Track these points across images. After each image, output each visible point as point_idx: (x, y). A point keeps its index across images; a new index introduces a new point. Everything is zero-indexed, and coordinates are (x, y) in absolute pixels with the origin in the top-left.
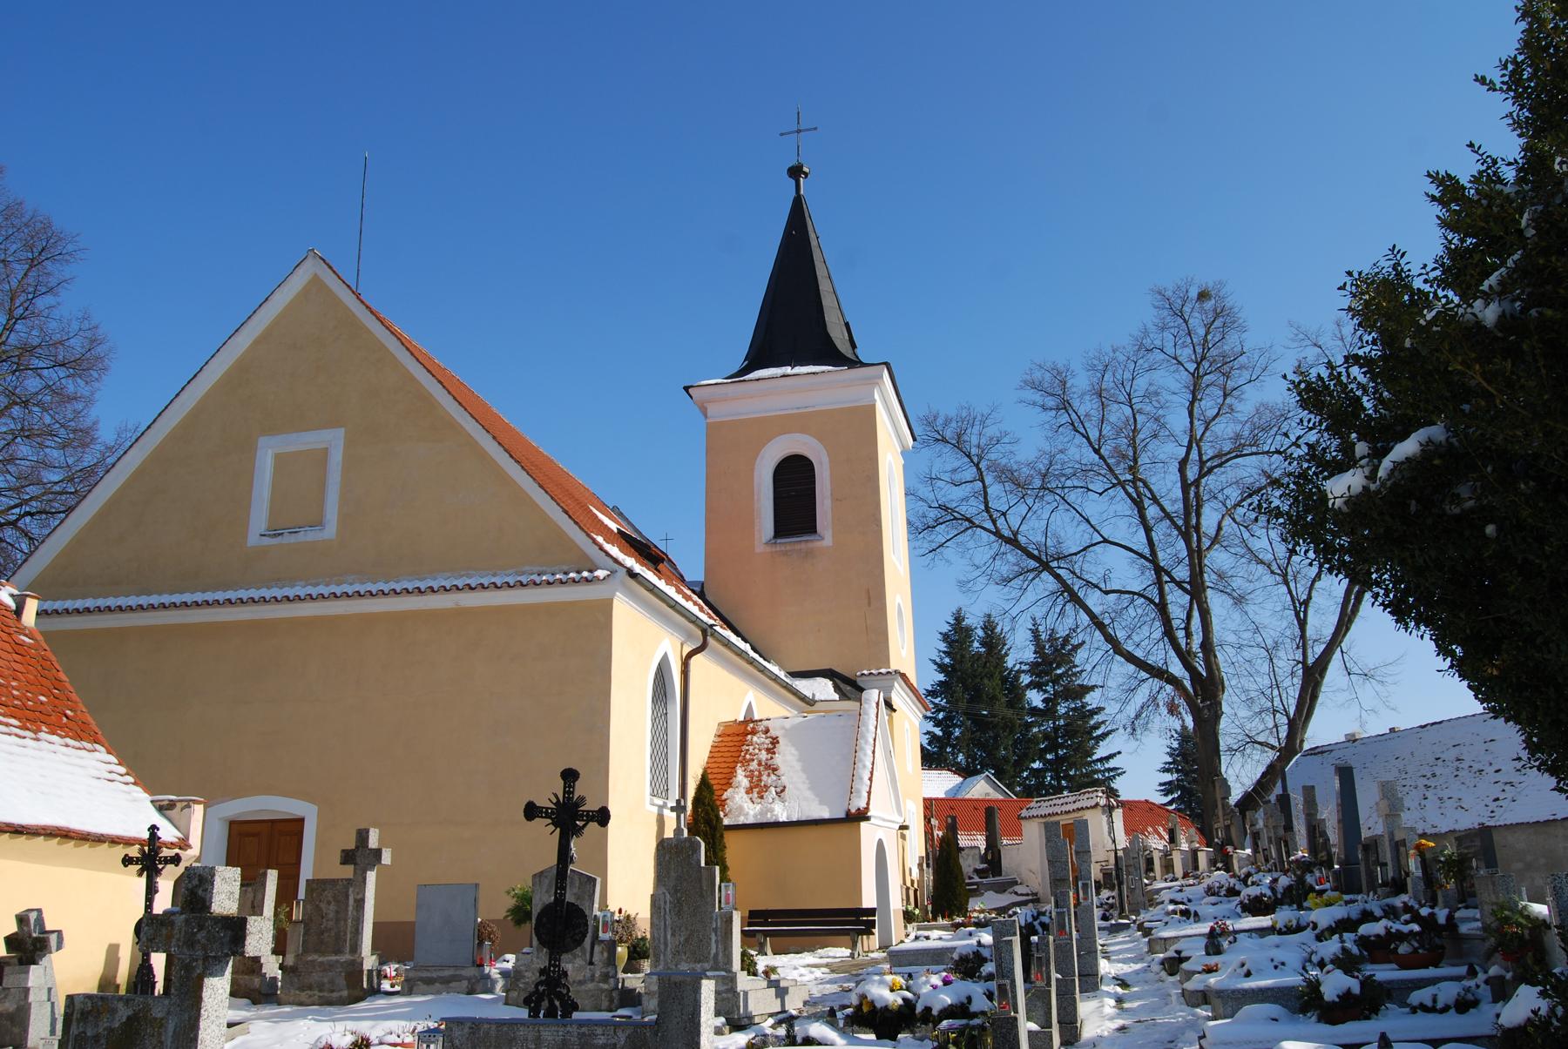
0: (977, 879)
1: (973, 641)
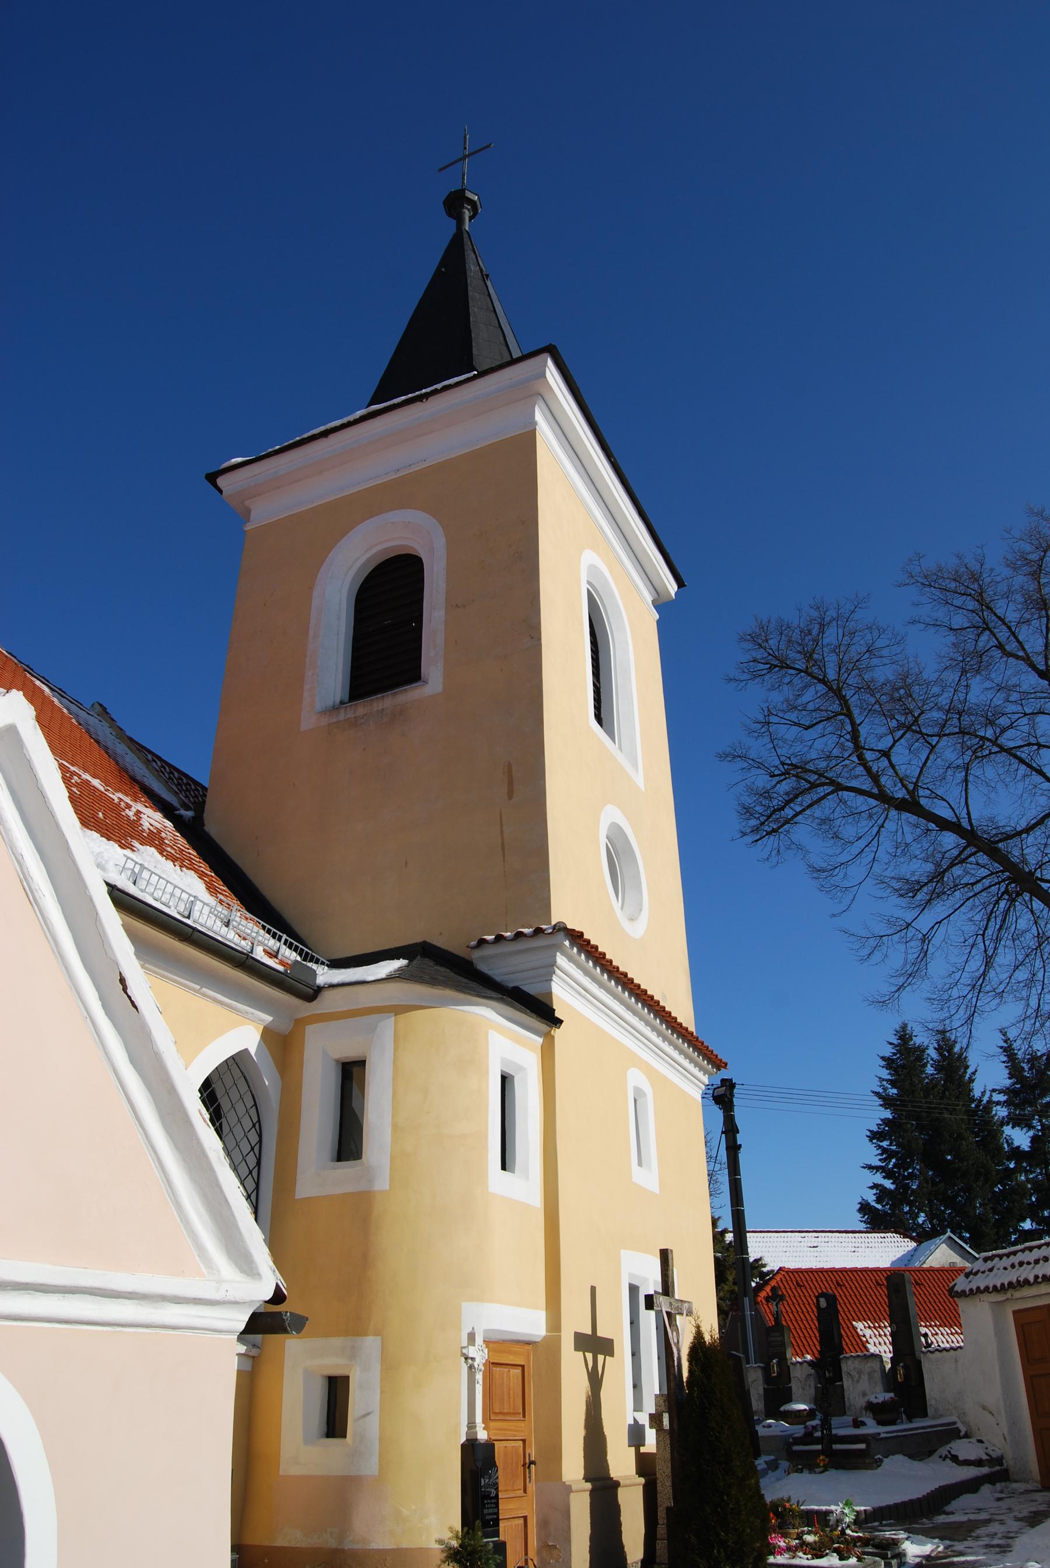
0: (871, 1427)
1: (925, 1065)
